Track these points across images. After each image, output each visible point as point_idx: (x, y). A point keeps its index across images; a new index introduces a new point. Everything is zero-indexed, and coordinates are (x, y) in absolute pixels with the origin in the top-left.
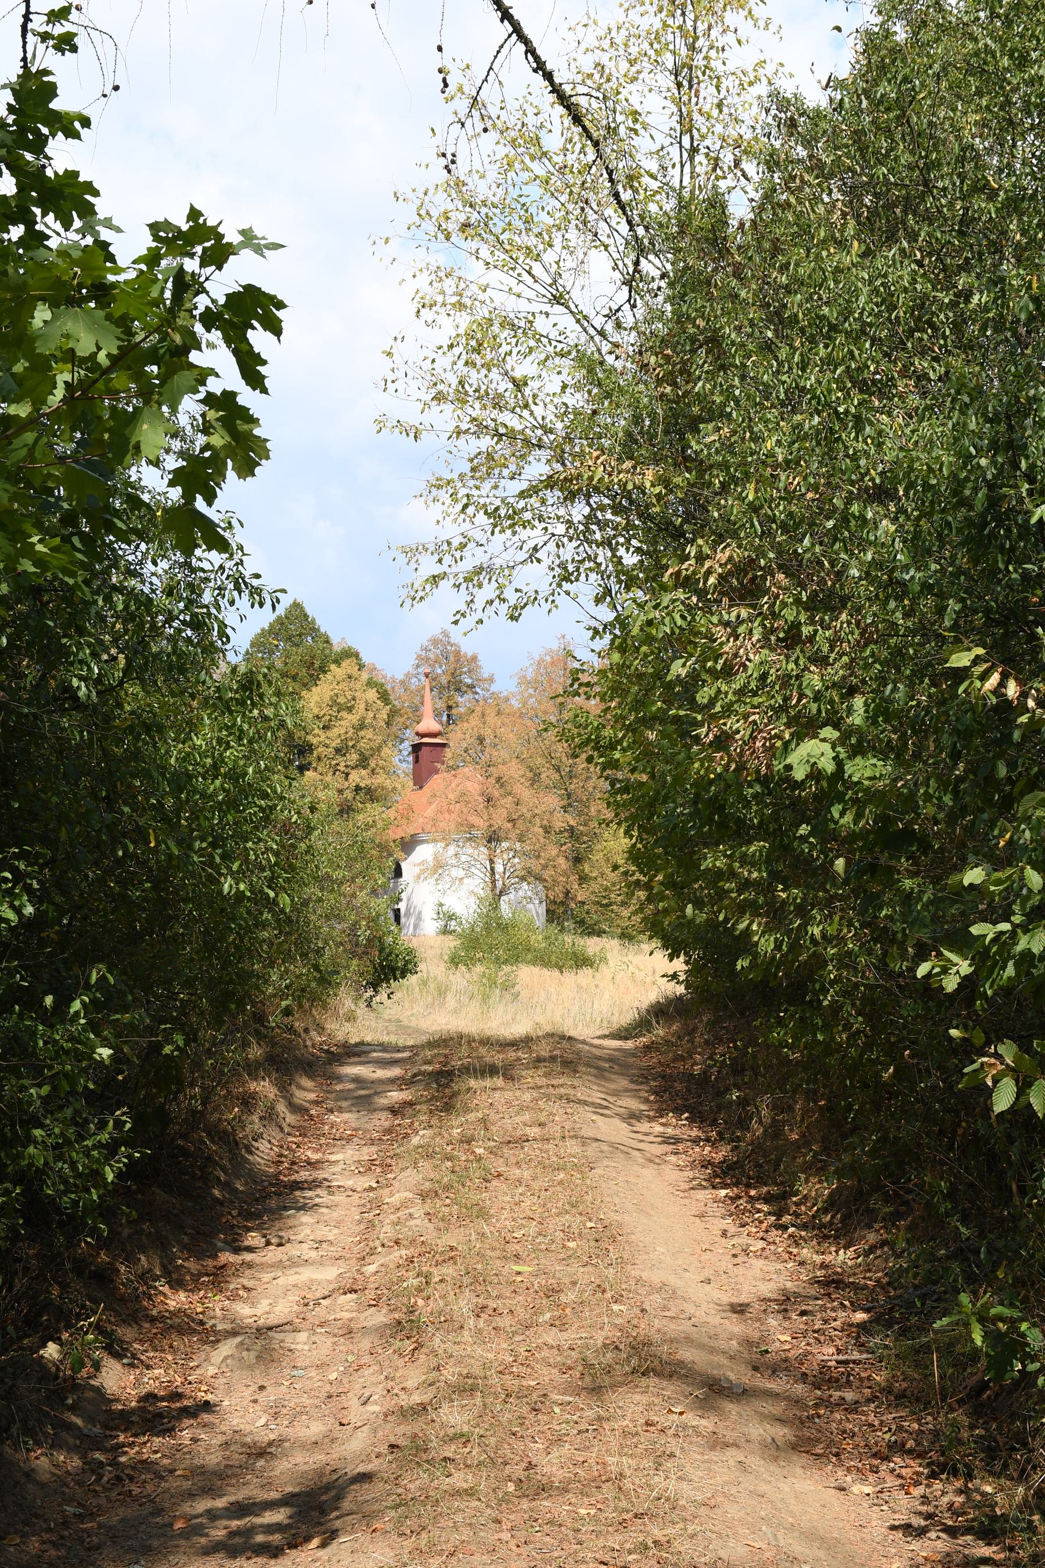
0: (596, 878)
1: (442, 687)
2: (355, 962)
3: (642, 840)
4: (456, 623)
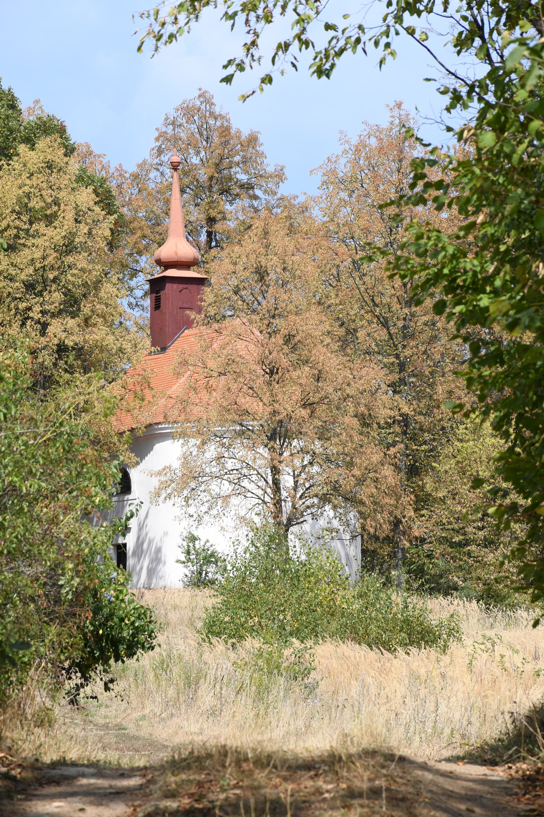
0: (443, 500)
1: (200, 186)
2: (54, 629)
3: (523, 440)
4: (228, 80)
